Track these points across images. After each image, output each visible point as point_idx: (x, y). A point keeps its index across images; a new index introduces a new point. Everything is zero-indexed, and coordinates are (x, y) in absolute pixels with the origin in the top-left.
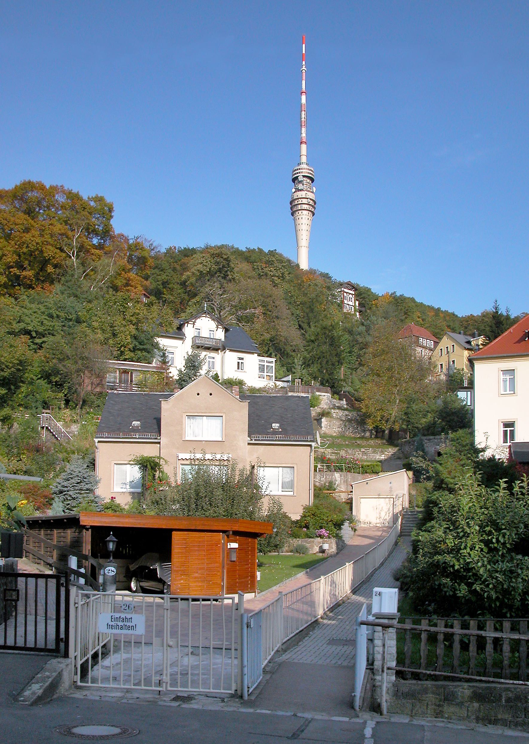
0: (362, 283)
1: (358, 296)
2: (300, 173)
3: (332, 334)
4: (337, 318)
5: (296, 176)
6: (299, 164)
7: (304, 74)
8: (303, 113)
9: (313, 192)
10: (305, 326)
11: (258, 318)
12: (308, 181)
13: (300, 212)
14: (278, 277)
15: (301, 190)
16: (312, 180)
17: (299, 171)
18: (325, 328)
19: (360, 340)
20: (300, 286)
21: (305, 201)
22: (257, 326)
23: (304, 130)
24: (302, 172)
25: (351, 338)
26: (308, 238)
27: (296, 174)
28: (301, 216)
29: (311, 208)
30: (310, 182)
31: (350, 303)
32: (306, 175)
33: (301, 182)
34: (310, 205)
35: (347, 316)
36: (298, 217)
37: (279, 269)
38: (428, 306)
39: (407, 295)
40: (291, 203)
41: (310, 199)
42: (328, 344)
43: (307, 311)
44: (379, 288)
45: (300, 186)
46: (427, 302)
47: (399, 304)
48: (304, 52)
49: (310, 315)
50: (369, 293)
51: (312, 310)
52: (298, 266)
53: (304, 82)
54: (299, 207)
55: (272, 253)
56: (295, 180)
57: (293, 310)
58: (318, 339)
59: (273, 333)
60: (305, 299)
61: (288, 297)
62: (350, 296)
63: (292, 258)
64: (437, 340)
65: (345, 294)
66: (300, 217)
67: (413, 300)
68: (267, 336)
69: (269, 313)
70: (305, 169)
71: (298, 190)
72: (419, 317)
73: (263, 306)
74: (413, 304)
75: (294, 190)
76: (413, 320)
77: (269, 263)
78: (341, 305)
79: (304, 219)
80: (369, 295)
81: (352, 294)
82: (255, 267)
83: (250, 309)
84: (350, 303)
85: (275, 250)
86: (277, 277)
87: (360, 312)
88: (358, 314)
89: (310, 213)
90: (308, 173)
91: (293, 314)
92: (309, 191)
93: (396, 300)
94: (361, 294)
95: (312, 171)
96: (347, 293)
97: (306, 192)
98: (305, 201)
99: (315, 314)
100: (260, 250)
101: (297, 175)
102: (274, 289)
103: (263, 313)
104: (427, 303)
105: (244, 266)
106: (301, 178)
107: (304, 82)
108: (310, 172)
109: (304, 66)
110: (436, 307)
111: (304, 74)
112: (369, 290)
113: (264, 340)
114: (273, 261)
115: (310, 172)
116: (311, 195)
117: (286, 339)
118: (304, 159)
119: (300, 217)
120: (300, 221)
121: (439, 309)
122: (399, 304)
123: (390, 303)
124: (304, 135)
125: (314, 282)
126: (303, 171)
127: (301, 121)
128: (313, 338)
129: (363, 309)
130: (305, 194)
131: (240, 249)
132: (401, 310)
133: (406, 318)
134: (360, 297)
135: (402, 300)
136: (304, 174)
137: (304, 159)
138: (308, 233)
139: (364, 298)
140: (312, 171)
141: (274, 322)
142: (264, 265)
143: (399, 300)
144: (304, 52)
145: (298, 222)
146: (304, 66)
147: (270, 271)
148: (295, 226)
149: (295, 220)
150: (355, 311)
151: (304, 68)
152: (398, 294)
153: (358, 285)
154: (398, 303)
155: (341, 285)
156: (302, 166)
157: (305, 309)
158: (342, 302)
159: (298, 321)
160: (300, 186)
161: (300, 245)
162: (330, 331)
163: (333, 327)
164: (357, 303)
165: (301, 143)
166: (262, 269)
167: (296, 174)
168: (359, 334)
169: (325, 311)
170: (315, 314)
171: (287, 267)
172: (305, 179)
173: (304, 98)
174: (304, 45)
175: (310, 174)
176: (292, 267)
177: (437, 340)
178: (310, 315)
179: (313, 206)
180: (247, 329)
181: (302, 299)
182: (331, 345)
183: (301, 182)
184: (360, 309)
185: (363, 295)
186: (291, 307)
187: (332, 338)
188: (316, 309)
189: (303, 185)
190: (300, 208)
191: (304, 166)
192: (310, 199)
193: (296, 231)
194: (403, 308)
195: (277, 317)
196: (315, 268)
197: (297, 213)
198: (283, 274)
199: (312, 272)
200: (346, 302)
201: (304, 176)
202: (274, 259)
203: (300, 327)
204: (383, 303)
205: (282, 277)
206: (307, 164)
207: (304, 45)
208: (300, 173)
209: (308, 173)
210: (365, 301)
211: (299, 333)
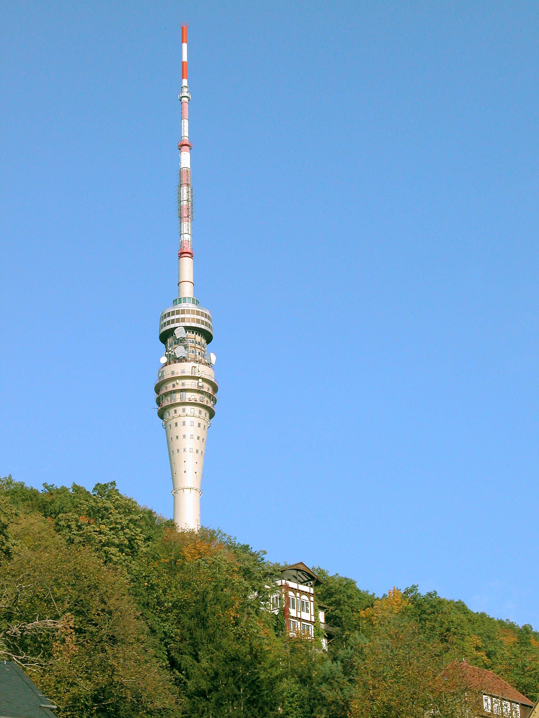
0: (334, 567)
1: (324, 599)
2: (178, 320)
3: (253, 674)
4: (274, 647)
5: (168, 327)
6: (177, 301)
7: (186, 106)
8: (184, 189)
9: (209, 364)
10: (187, 660)
11: (64, 641)
12: (199, 338)
13: (179, 409)
14: (120, 547)
15: (183, 360)
16: (208, 337)
17: (177, 317)
18: (233, 659)
19: (330, 695)
20: (173, 567)
21: (190, 384)
22: (61, 662)
23: (186, 227)
24: (183, 320)
25: (305, 692)
26: (199, 469)
27: (168, 323)
28: (182, 419)
29: (206, 401)
30: (204, 341)
31: (305, 616)
32: (194, 325)
33: (181, 341)
34: (202, 392)
35: (297, 646)
36: (175, 421)
37: (122, 529)
38: (501, 622)
39: (445, 594)
40: (158, 389)
41: (204, 380)
42: (242, 701)
43: (192, 623)
44: (377, 578)
45: (180, 351)
46: (496, 613)
47: (424, 616)
48: (185, 59)
49: (199, 633)
50: (350, 592)
51: (203, 623)
52: (171, 525)
53: (185, 124)
54: (178, 398)
55: (105, 490)
56: (166, 336)
57: (154, 620)
58: (216, 689)
59: (102, 679)
60: (187, 595)
61: (141, 590)
62: (304, 597)
63: (162, 513)
64: (529, 702)
65: (291, 594)
66: (180, 421)
67: (461, 607)
68: (86, 688)
69: (92, 629)
70: (190, 314)
71: (174, 359)
72: (478, 648)
73: (79, 613)
74: (462, 616)
75: (164, 360)
76: (463, 652)
77: (97, 514)
78: (280, 623)
79: (189, 424)
80: (350, 597)
81: (308, 594)
82: (62, 523)
83: (41, 618)
84: (306, 614)
85: (114, 483)
86: (118, 546)
87: (329, 637)
88: (324, 642)
89: (204, 411)
90: (198, 321)
91: (153, 631)
92: (200, 362)
93: (419, 606)
94: (331, 595)
95: (206, 316)
96: (292, 589)
97: (193, 364)
98: (190, 384)
99: (211, 631)
100: (77, 489)
101: (172, 326)
102: (105, 568)
103: (76, 630)
104: (495, 614)
105: (36, 522)
106: (180, 333)
107: (185, 124)
108: (203, 319)
109: (186, 90)
110: (520, 624)
111: (186, 106)
112: (350, 584)
113: (75, 699)
114: (106, 509)
115: (203, 319)
116: (205, 371)
117: (138, 697)
118: (187, 290)
119: (180, 421)
120: (181, 430)
121: (527, 630)
122: (424, 616)
123: (403, 613)
124: (187, 237)
125: (210, 559)
126: (187, 316)
127: (180, 209)
128: (204, 685)
129: (335, 630)
130: (190, 370)
131: (28, 485)
132: (433, 629)
133: (447, 650)
134: (328, 601)
135: (432, 606)
136: (188, 324)
137: (187, 290)
138: (198, 457)
139: (338, 603)
140: (206, 316)
141: (103, 650)
142: (83, 520)
143: (426, 606)
144: (185, 59)
145: (174, 432)
146: (186, 90)
147: (100, 533)
148: (169, 441)
149: (166, 427)
150: (318, 634)
151: (186, 94)
152: (423, 591)
153: (322, 572)
154: (424, 612)
155: (283, 572)
156: (183, 306)
157: (185, 620)
158: (284, 612)
159: (168, 651)
160: (180, 351)
161: (180, 485)
162: (247, 667)
163: (256, 657)
164: (322, 616)
165: (181, 254)
166: (80, 528)
167: (168, 323)
168: (325, 679)
169: (237, 624)
170: (211, 631)
171: (143, 523)
172: (191, 335)
173: (186, 159)
174: (185, 45)
175: (203, 323)
176: (157, 528)
177: (529, 702)
178: (199, 633)
179: (209, 396)
180: (33, 669)
181: (177, 594)
182: (251, 702)
183: (181, 341)
184: (330, 629)
185: (333, 596)
186: (149, 613)
187: (254, 685)
188: (212, 620)
189: (186, 347)
190: (178, 401)
191: (191, 306)
192: (204, 380)
193: (170, 453)
194: (437, 625)
195: (113, 640)
196: (213, 526)
197: (172, 411)
198: (130, 540)
199: (207, 536)
200: (293, 612)
201: (187, 328)
202: (109, 504)
203: (173, 664)
204: (386, 614)
205: (131, 547)
206: (196, 302)
207: (185, 45)
208: (178, 320)
209: (198, 321)
210: (341, 610)
211: (167, 675)
